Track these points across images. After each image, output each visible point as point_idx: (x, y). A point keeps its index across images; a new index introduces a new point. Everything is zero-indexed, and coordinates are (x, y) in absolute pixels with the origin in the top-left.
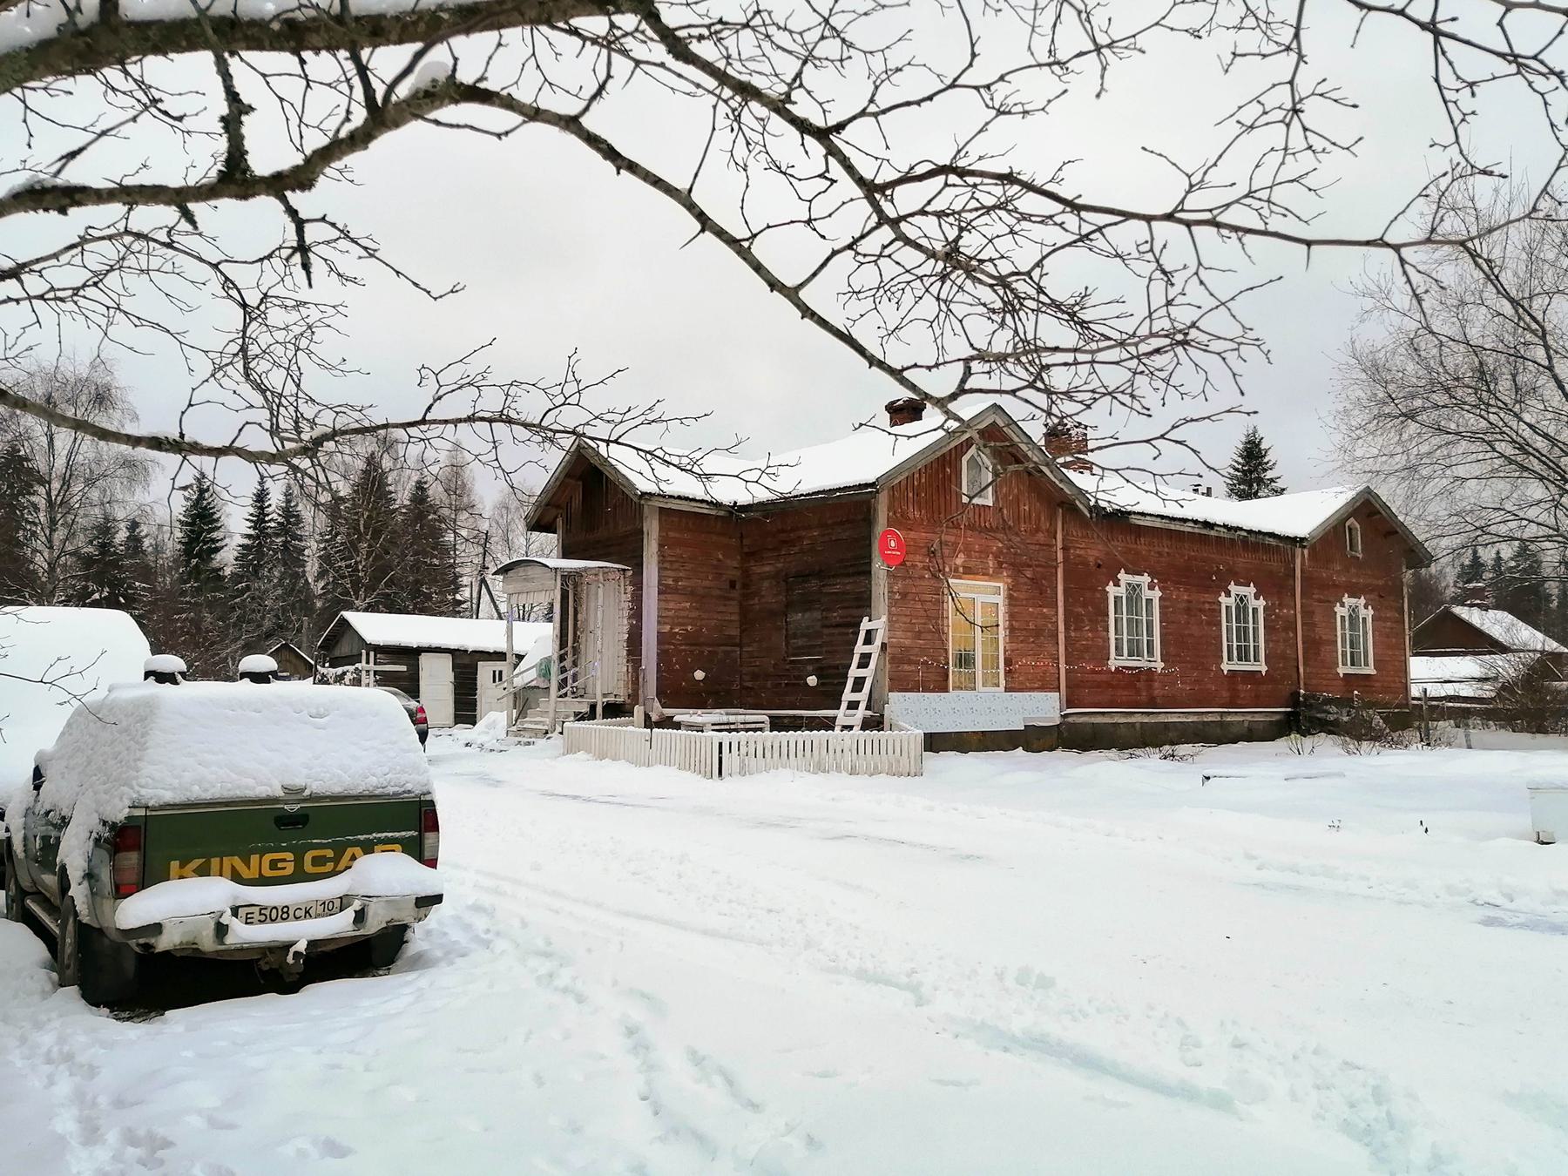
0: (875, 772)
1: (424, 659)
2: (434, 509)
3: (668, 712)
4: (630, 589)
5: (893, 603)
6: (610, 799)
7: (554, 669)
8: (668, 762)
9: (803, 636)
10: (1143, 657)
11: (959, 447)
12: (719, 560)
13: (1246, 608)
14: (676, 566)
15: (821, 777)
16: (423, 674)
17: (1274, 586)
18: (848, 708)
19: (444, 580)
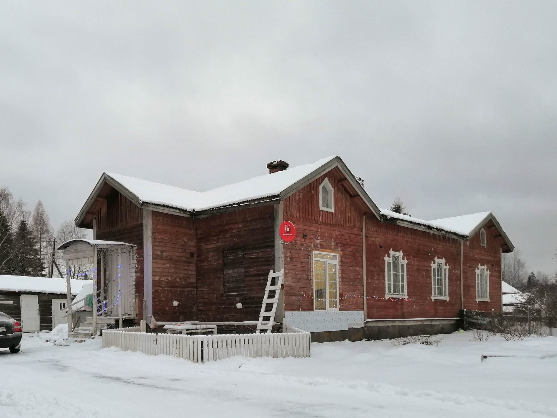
0: (285, 356)
1: (23, 298)
2: (29, 233)
3: (160, 323)
4: (136, 257)
5: (286, 263)
6: (141, 381)
7: (95, 300)
8: (168, 352)
9: (233, 281)
10: (399, 292)
11: (318, 180)
12: (184, 242)
13: (441, 269)
14: (162, 244)
15: (258, 360)
16: (22, 305)
17: (452, 260)
18: (264, 320)
19: (36, 265)
